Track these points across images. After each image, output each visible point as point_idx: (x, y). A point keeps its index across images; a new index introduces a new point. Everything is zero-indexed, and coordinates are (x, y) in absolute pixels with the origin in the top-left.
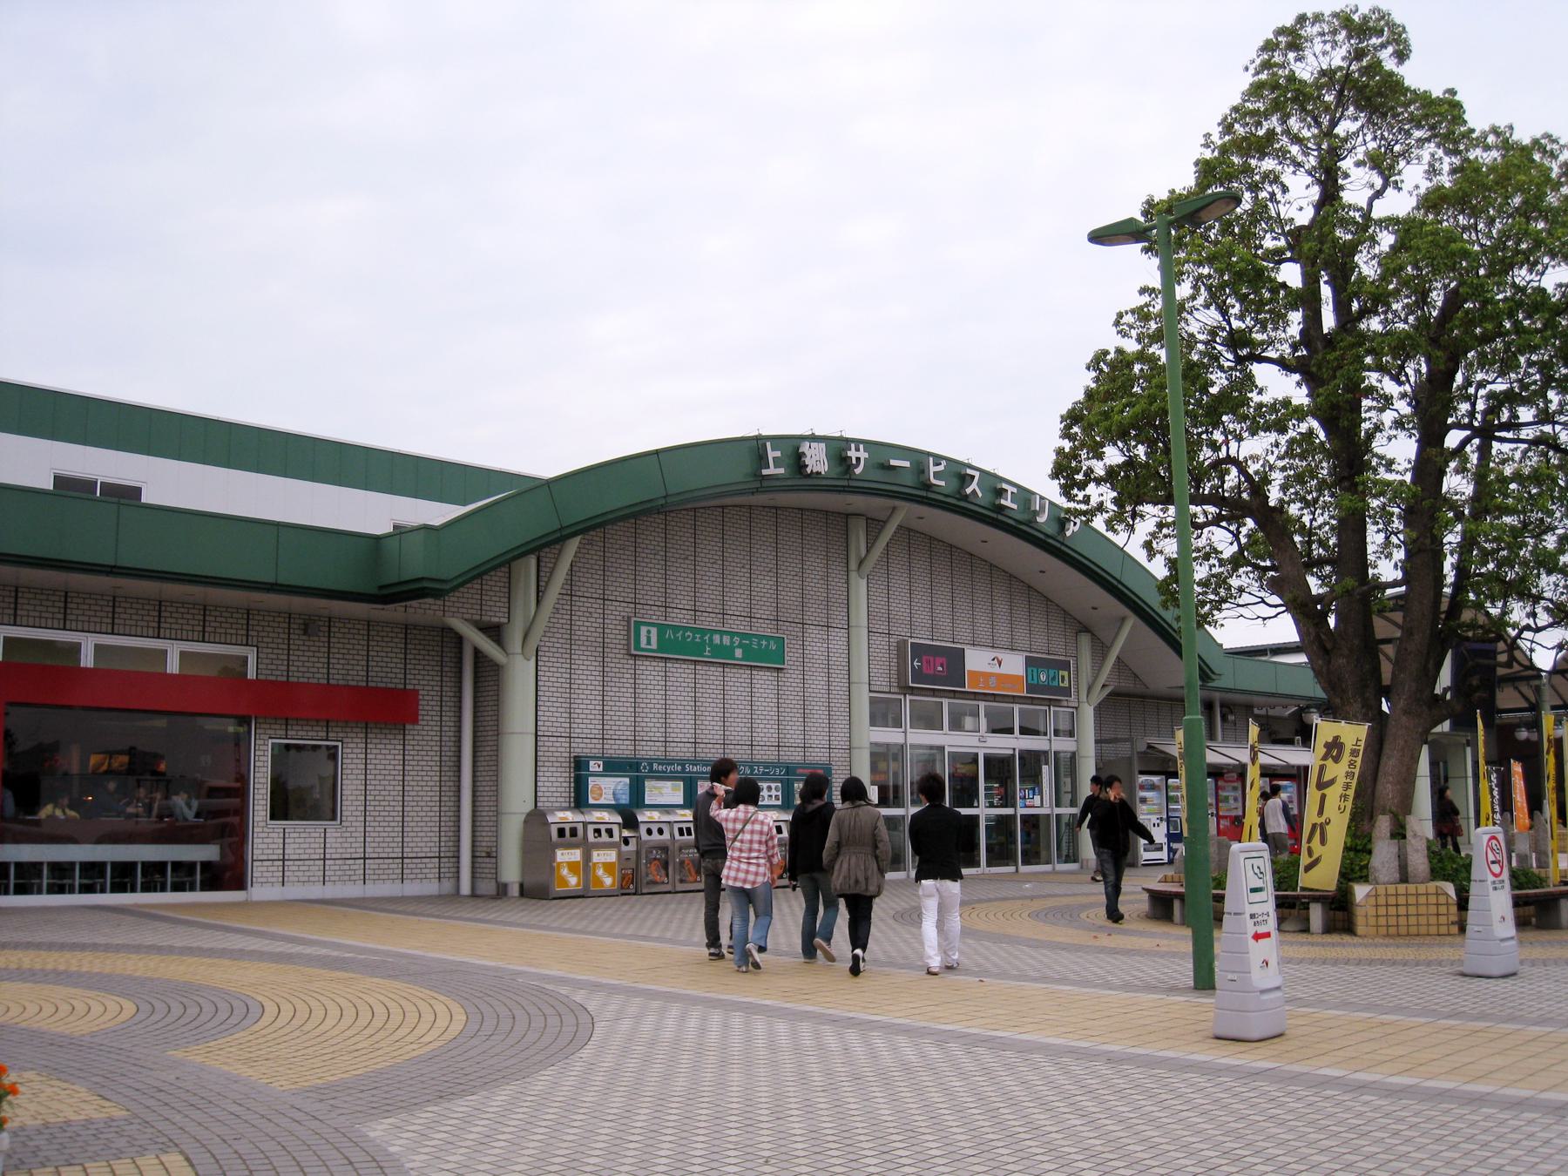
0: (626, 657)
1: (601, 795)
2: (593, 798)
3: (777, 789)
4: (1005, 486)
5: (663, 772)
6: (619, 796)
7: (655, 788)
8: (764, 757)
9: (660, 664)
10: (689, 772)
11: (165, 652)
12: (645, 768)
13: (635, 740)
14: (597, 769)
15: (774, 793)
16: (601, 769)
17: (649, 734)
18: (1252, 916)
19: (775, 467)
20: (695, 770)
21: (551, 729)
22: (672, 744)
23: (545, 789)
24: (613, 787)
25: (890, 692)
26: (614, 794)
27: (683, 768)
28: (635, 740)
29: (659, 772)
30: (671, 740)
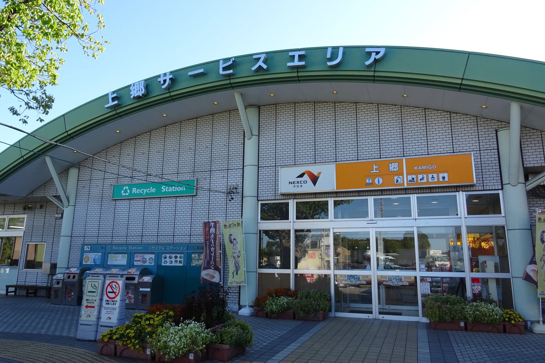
0: (111, 201)
1: (88, 260)
2: (85, 262)
3: (180, 257)
4: (291, 54)
5: (117, 250)
6: (96, 261)
7: (113, 257)
8: (104, 242)
9: (127, 202)
10: (131, 250)
11: (327, 201)
12: (109, 248)
13: (174, 235)
14: (88, 249)
15: (178, 259)
16: (89, 249)
17: (119, 233)
18: (87, 300)
19: (260, 66)
20: (134, 248)
21: (185, 232)
22: (87, 238)
23: (72, 258)
24: (94, 257)
25: (275, 200)
26: (94, 260)
27: (128, 248)
28: (174, 235)
29: (115, 250)
30: (145, 235)
